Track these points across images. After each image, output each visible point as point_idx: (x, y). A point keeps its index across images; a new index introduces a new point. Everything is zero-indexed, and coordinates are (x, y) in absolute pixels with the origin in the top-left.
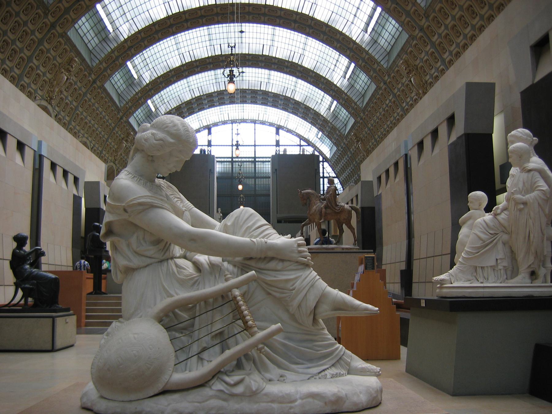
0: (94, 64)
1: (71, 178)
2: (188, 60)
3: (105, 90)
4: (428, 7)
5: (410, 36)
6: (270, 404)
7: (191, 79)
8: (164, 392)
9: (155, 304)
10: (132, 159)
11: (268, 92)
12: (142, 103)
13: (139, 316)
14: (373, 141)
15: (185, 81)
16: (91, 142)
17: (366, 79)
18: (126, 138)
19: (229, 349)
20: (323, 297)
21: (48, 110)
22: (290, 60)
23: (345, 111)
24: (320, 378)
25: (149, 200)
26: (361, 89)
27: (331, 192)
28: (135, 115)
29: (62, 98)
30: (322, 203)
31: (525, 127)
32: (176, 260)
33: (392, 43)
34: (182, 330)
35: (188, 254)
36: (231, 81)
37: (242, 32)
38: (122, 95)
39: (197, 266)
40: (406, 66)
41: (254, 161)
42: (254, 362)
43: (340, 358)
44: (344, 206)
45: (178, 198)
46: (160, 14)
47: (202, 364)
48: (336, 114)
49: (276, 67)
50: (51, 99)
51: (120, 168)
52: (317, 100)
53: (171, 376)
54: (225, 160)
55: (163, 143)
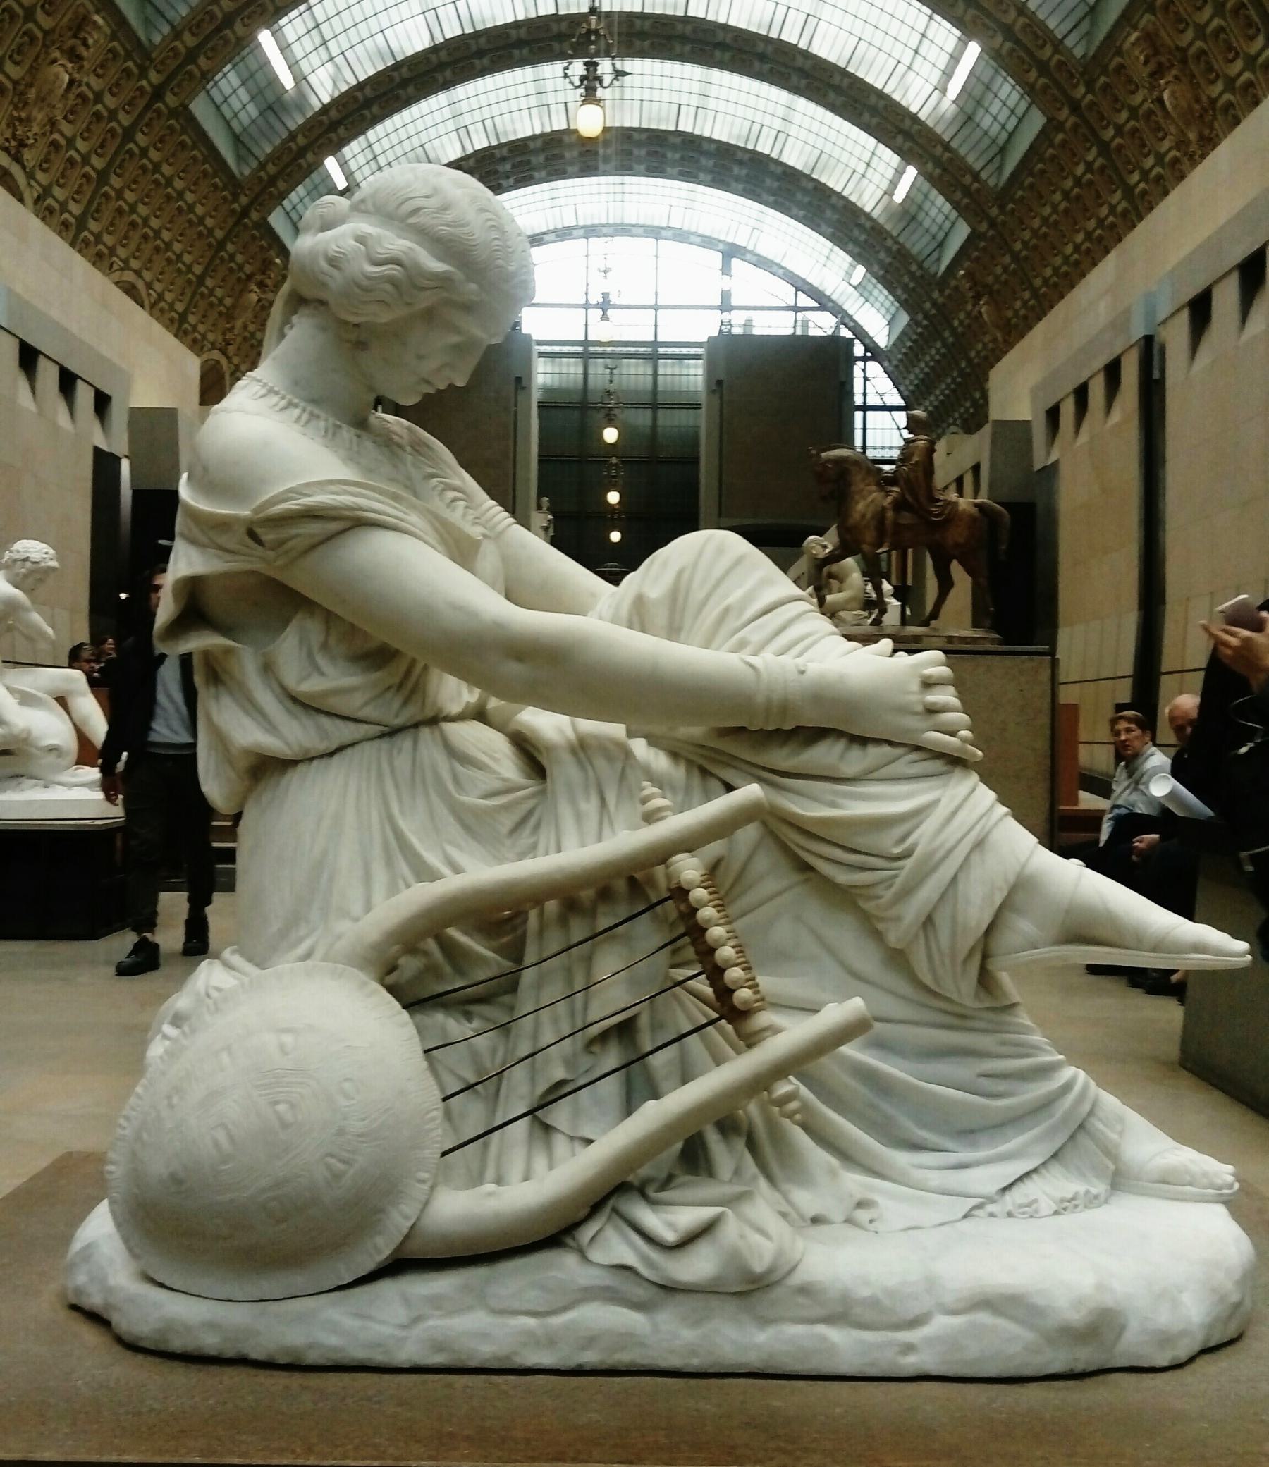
0: (157, 39)
1: (84, 396)
3: (192, 120)
6: (821, 1329)
7: (461, 91)
8: (401, 1265)
9: (368, 908)
11: (701, 138)
12: (310, 165)
13: (302, 949)
15: (441, 98)
17: (1015, 96)
18: (259, 277)
19: (656, 1096)
20: (1020, 892)
21: (14, 181)
23: (940, 200)
24: (1010, 1215)
25: (347, 499)
26: (996, 127)
27: (916, 459)
28: (285, 202)
29: (55, 144)
30: (888, 493)
31: (499, 345)
32: (448, 727)
34: (461, 1003)
35: (493, 703)
36: (590, 96)
38: (245, 139)
40: (1149, 51)
41: (653, 353)
42: (752, 1145)
43: (1081, 1126)
44: (956, 504)
45: (455, 489)
48: (913, 210)
49: (727, 56)
50: (22, 144)
51: (243, 368)
53: (426, 1204)
54: (565, 349)
55: (407, 281)
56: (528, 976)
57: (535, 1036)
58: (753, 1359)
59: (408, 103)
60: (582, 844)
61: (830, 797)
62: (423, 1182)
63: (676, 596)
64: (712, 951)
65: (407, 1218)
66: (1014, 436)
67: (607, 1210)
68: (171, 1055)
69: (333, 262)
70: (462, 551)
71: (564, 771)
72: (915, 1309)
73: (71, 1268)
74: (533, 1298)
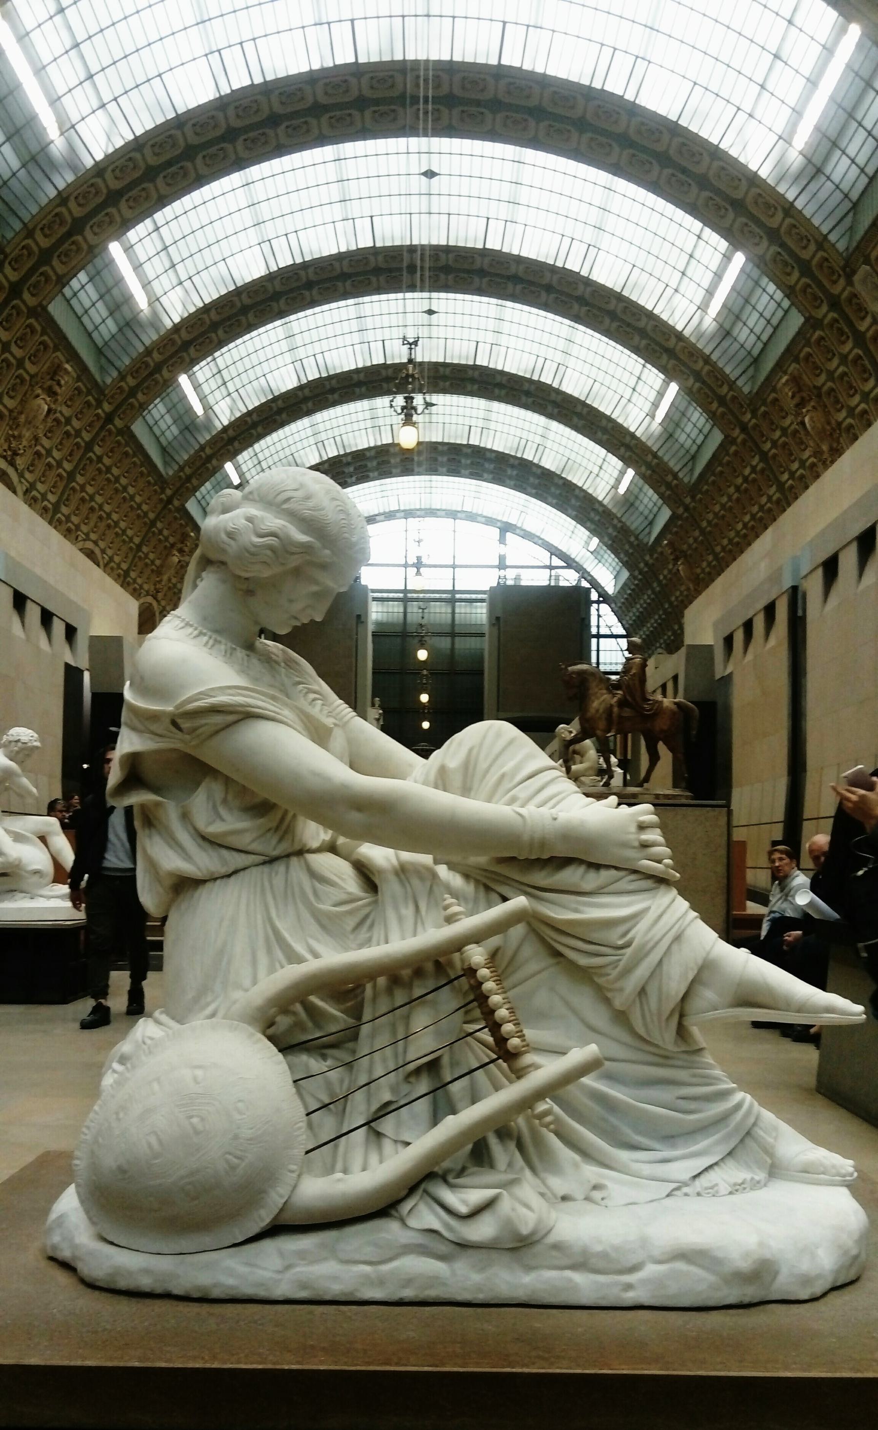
0: (109, 381)
1: (58, 628)
2: (313, 375)
3: (133, 437)
4: (854, 251)
5: (807, 320)
6: (568, 1273)
8: (276, 1229)
9: (255, 982)
10: (195, 586)
12: (214, 468)
14: (710, 558)
16: (103, 551)
17: (703, 420)
18: (179, 546)
19: (454, 1112)
20: (706, 970)
22: (535, 378)
23: (651, 492)
24: (699, 1194)
26: (689, 442)
27: (634, 671)
28: (197, 494)
29: (38, 453)
30: (614, 695)
32: (311, 857)
33: (765, 338)
35: (341, 840)
36: (408, 420)
37: (430, 312)
39: (368, 876)
40: (795, 389)
41: (452, 598)
42: (520, 1146)
43: (748, 1133)
44: (661, 702)
46: (250, 268)
47: (380, 1148)
48: (632, 499)
49: (503, 392)
50: (15, 454)
51: (168, 608)
52: (590, 467)
53: (295, 1187)
54: (391, 595)
55: (281, 548)
56: (365, 1029)
57: (370, 1071)
58: (521, 1295)
59: (282, 425)
60: (403, 937)
61: (574, 906)
62: (293, 1172)
63: (468, 767)
64: (493, 1011)
65: (281, 1196)
66: (702, 653)
67: (420, 1191)
68: (118, 1084)
69: (231, 535)
70: (320, 735)
71: (390, 887)
72: (634, 1259)
73: (49, 1231)
74: (369, 1252)
